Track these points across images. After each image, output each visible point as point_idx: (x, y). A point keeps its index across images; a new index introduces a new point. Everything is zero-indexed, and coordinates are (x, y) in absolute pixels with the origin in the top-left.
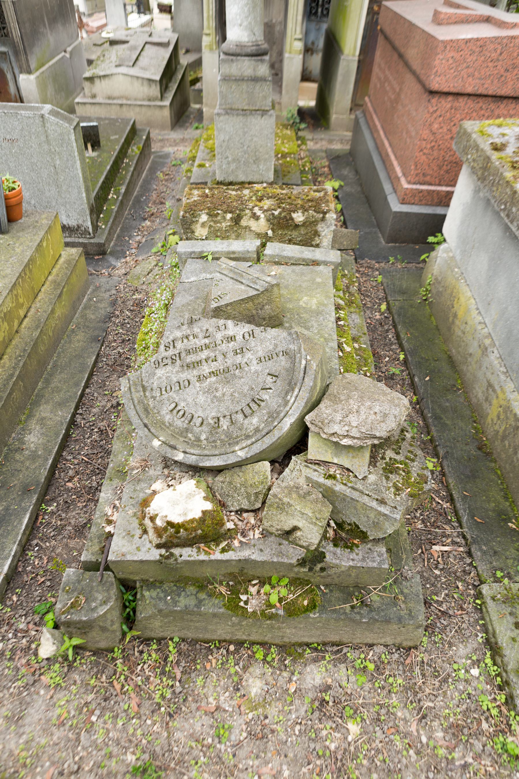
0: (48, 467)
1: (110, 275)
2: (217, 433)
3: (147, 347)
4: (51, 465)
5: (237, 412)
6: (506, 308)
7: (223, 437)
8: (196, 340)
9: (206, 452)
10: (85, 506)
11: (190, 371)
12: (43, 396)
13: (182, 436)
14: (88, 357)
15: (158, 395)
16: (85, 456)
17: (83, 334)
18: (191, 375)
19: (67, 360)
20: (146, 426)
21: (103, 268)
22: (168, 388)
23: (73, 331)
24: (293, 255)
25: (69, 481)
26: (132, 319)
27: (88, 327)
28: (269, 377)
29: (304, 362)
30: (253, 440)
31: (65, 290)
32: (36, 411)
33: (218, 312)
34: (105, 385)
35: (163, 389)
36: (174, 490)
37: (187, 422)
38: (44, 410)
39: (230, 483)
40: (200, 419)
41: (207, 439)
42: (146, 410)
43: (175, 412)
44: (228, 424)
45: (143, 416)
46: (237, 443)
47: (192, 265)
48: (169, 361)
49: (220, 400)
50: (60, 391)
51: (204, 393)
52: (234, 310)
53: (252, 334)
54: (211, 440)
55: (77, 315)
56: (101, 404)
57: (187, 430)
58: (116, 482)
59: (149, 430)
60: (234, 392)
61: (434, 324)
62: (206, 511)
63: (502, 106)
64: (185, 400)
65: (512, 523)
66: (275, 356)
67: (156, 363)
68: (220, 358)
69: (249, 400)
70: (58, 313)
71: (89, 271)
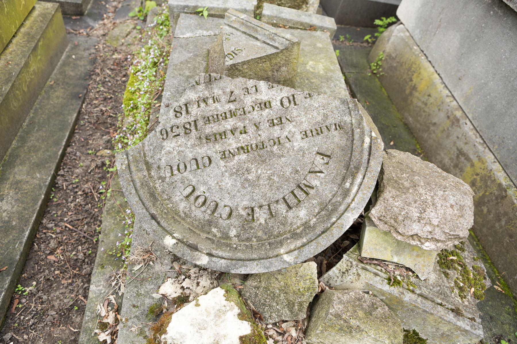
0: (24, 240)
1: (88, 35)
2: (251, 228)
3: (136, 107)
4: (29, 238)
5: (277, 202)
6: (486, 84)
7: (260, 234)
8: (217, 104)
9: (240, 255)
10: (71, 284)
11: (211, 145)
12: (18, 156)
13: (203, 231)
14: (68, 115)
15: (168, 175)
16: (69, 223)
17: (62, 90)
18: (213, 150)
19: (46, 117)
20: (153, 217)
21: (81, 28)
22: (182, 167)
23: (51, 87)
24: (291, 18)
25: (52, 253)
26: (113, 78)
27: (67, 83)
28: (319, 158)
29: (367, 140)
30: (305, 240)
31: (40, 43)
32: (10, 173)
33: (233, 71)
34: (88, 144)
35: (175, 168)
36: (197, 305)
37: (209, 212)
38: (19, 173)
39: (267, 289)
40: (227, 209)
41: (238, 236)
42: (153, 195)
43: (192, 198)
44: (265, 216)
45: (149, 204)
46: (281, 243)
47: (185, 20)
48: (181, 131)
49: (253, 184)
50: (38, 150)
51: (231, 175)
52: (251, 70)
53: (292, 100)
54: (244, 237)
55: (55, 71)
56: (85, 164)
57: (210, 223)
58: (109, 270)
59: (158, 223)
60: (273, 174)
61: (386, 94)
62: (246, 336)
64: (205, 183)
65: (497, 285)
66: (325, 130)
67: (164, 132)
68: (251, 129)
69: (293, 186)
70: (34, 67)
71: (66, 29)
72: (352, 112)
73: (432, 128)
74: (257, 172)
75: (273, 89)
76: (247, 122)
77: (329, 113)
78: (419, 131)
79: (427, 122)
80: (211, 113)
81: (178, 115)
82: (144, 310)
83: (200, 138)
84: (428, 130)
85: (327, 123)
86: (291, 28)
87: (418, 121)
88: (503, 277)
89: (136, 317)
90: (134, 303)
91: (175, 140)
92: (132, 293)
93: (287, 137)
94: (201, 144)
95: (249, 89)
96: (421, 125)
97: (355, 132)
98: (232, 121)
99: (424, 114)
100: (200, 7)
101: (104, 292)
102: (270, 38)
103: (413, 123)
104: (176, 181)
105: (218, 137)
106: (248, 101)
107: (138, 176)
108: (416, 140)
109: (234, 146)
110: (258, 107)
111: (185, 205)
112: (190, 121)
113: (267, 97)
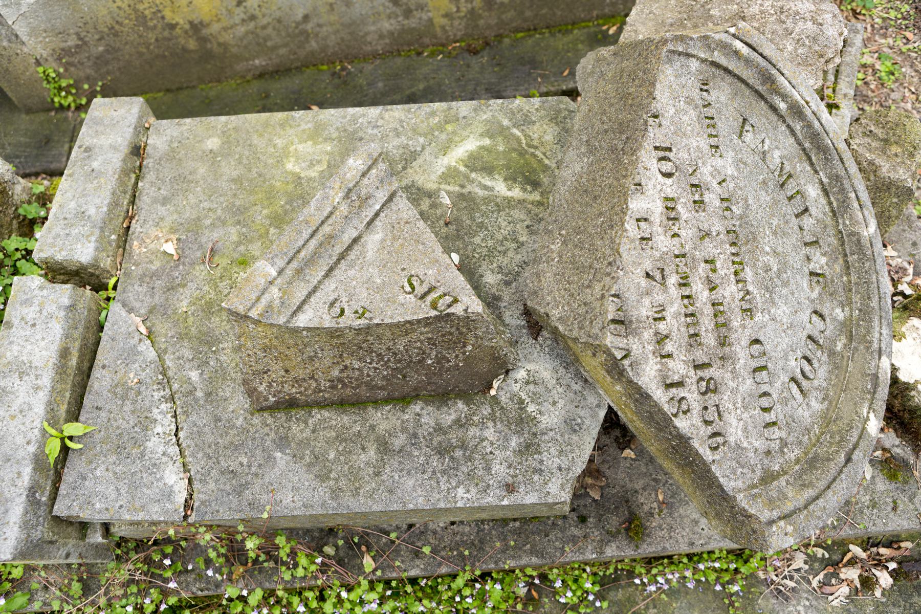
5: (801, 228)
8: (668, 314)
48: (712, 399)
53: (664, 152)
59: (855, 448)
65: (608, 29)
68: (709, 249)
72: (690, 51)
73: (309, 26)
74: (767, 253)
75: (643, 184)
76: (698, 253)
77: (685, 94)
78: (295, 53)
79: (290, 30)
80: (682, 329)
81: (684, 407)
82: (897, 488)
83: (722, 358)
84: (308, 35)
85: (700, 103)
86: (133, 202)
87: (274, 48)
88: (598, 17)
89: (910, 501)
90: (889, 509)
91: (726, 415)
92: (874, 517)
93: (720, 183)
94: (731, 358)
95: (643, 235)
96: (286, 45)
97: (717, 60)
98: (697, 285)
99: (269, 30)
100: (42, 445)
101: (808, 599)
102: (360, 207)
103: (270, 59)
104: (785, 416)
105: (721, 320)
106: (663, 243)
107: (795, 498)
108: (308, 67)
109: (733, 288)
110: (674, 225)
111: (813, 399)
112: (695, 379)
113: (658, 201)
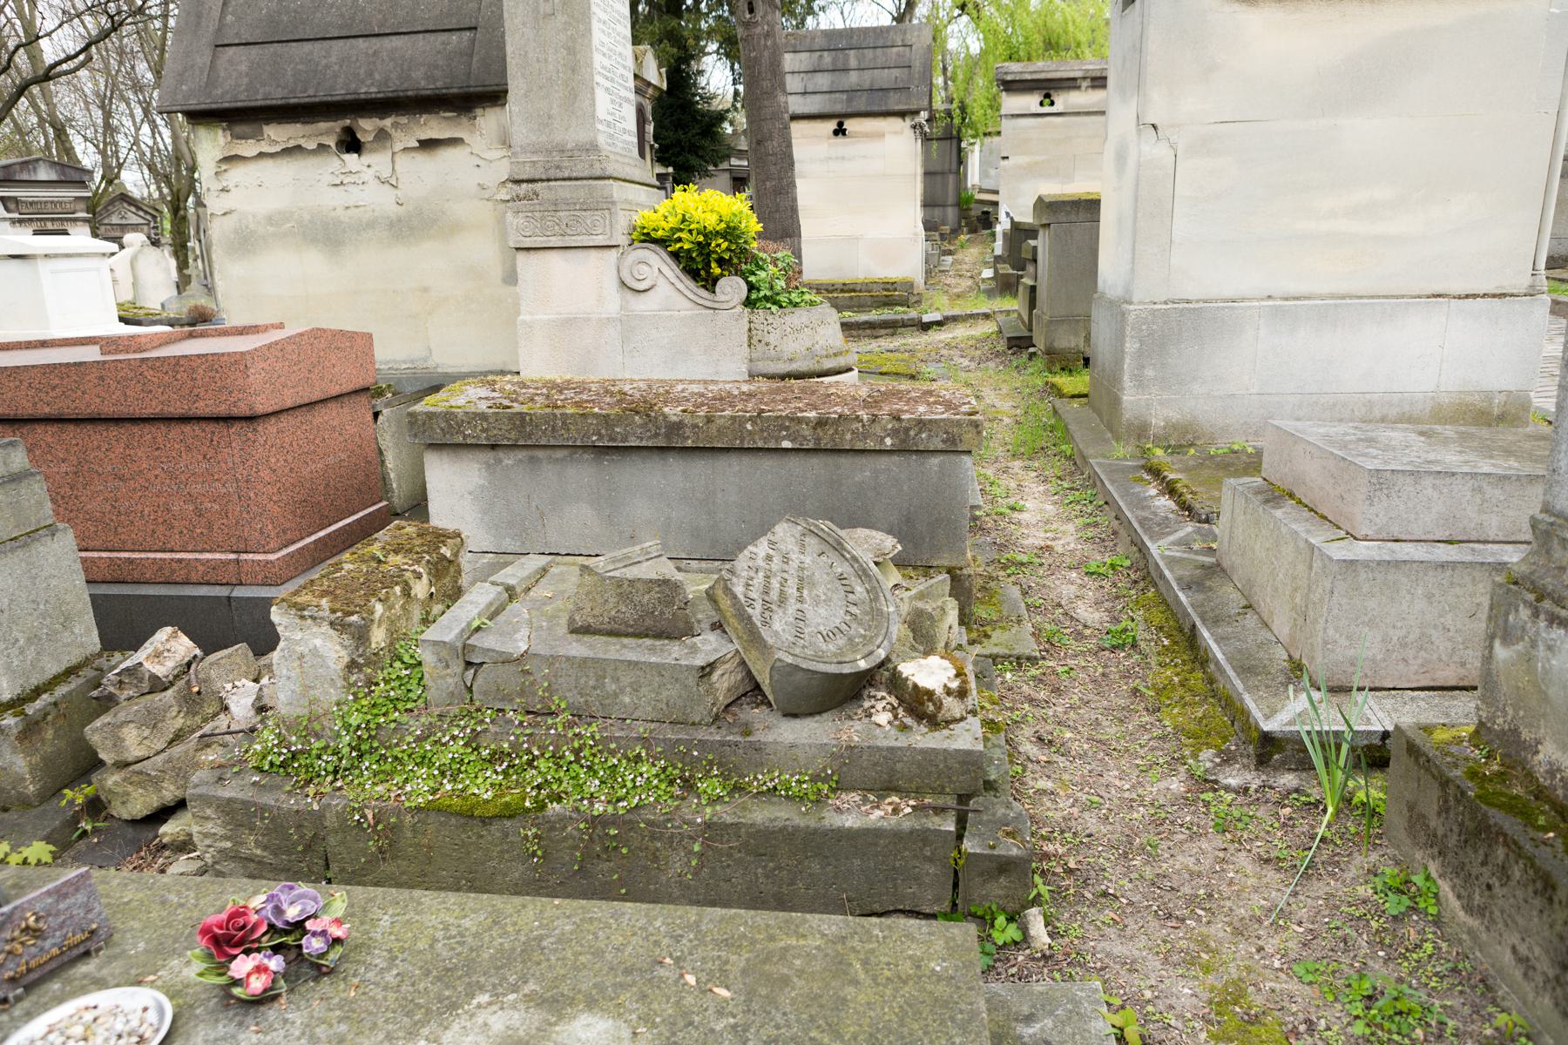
48: (767, 614)
53: (772, 543)
63: (346, 410)
